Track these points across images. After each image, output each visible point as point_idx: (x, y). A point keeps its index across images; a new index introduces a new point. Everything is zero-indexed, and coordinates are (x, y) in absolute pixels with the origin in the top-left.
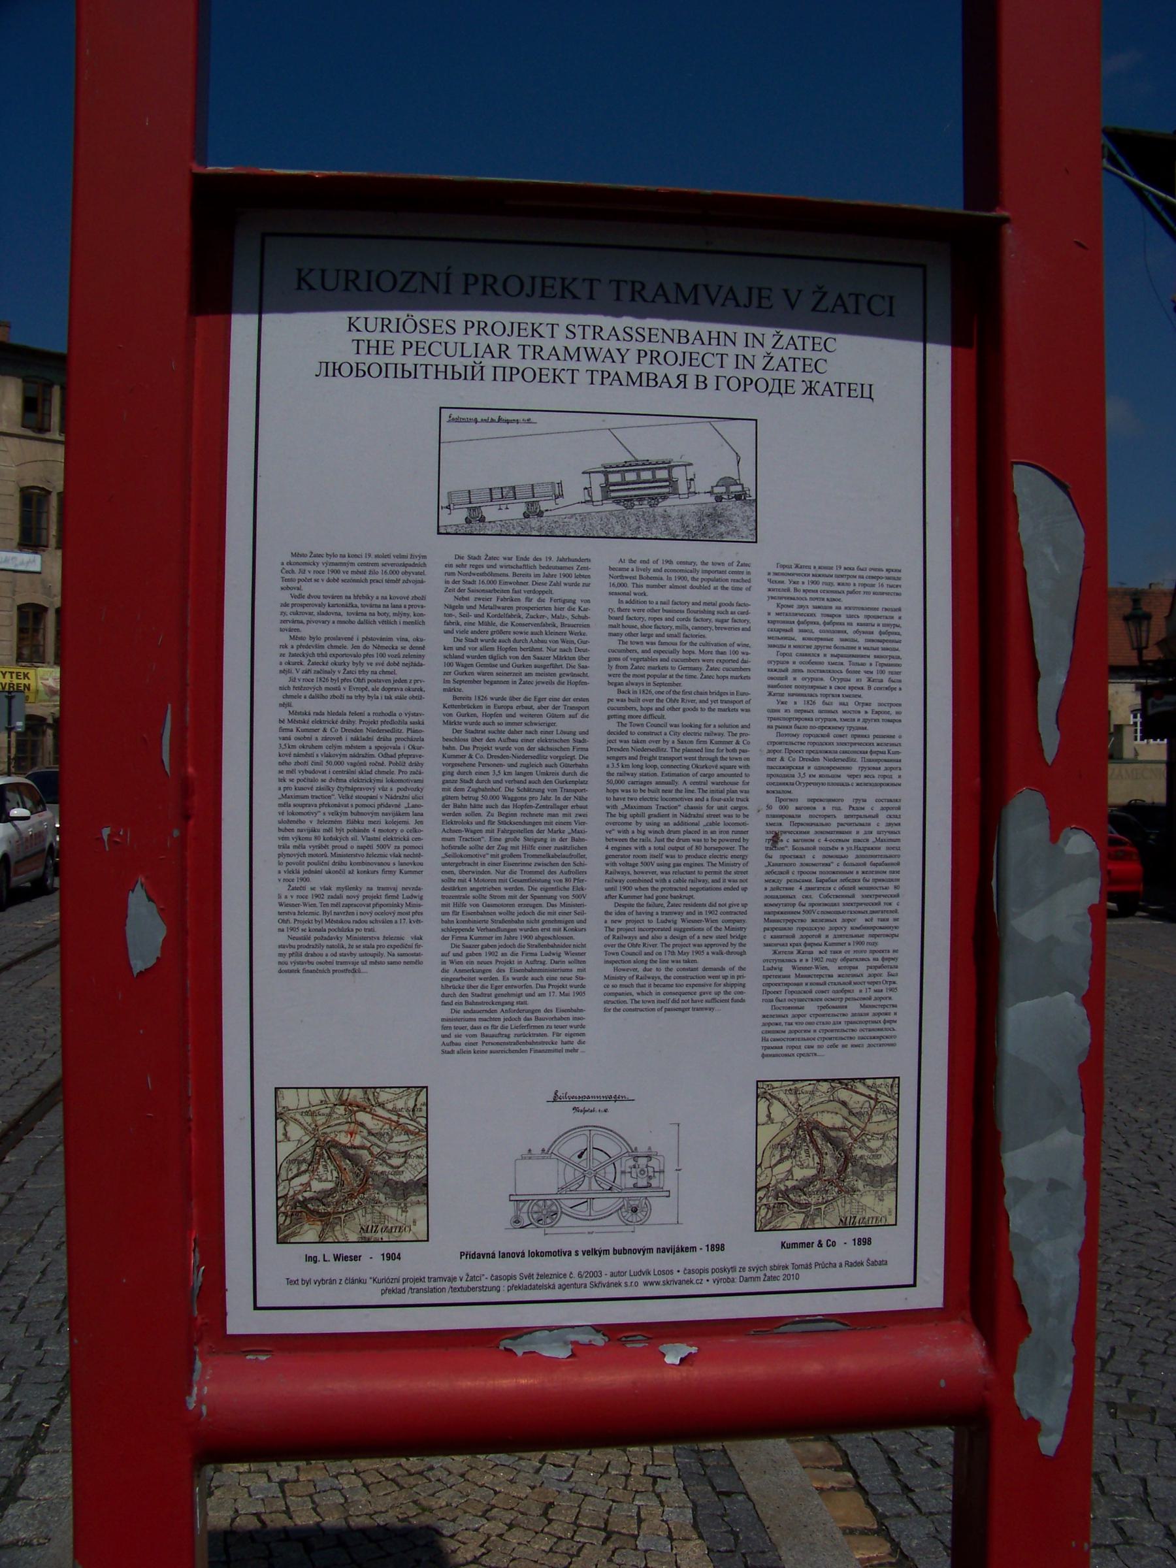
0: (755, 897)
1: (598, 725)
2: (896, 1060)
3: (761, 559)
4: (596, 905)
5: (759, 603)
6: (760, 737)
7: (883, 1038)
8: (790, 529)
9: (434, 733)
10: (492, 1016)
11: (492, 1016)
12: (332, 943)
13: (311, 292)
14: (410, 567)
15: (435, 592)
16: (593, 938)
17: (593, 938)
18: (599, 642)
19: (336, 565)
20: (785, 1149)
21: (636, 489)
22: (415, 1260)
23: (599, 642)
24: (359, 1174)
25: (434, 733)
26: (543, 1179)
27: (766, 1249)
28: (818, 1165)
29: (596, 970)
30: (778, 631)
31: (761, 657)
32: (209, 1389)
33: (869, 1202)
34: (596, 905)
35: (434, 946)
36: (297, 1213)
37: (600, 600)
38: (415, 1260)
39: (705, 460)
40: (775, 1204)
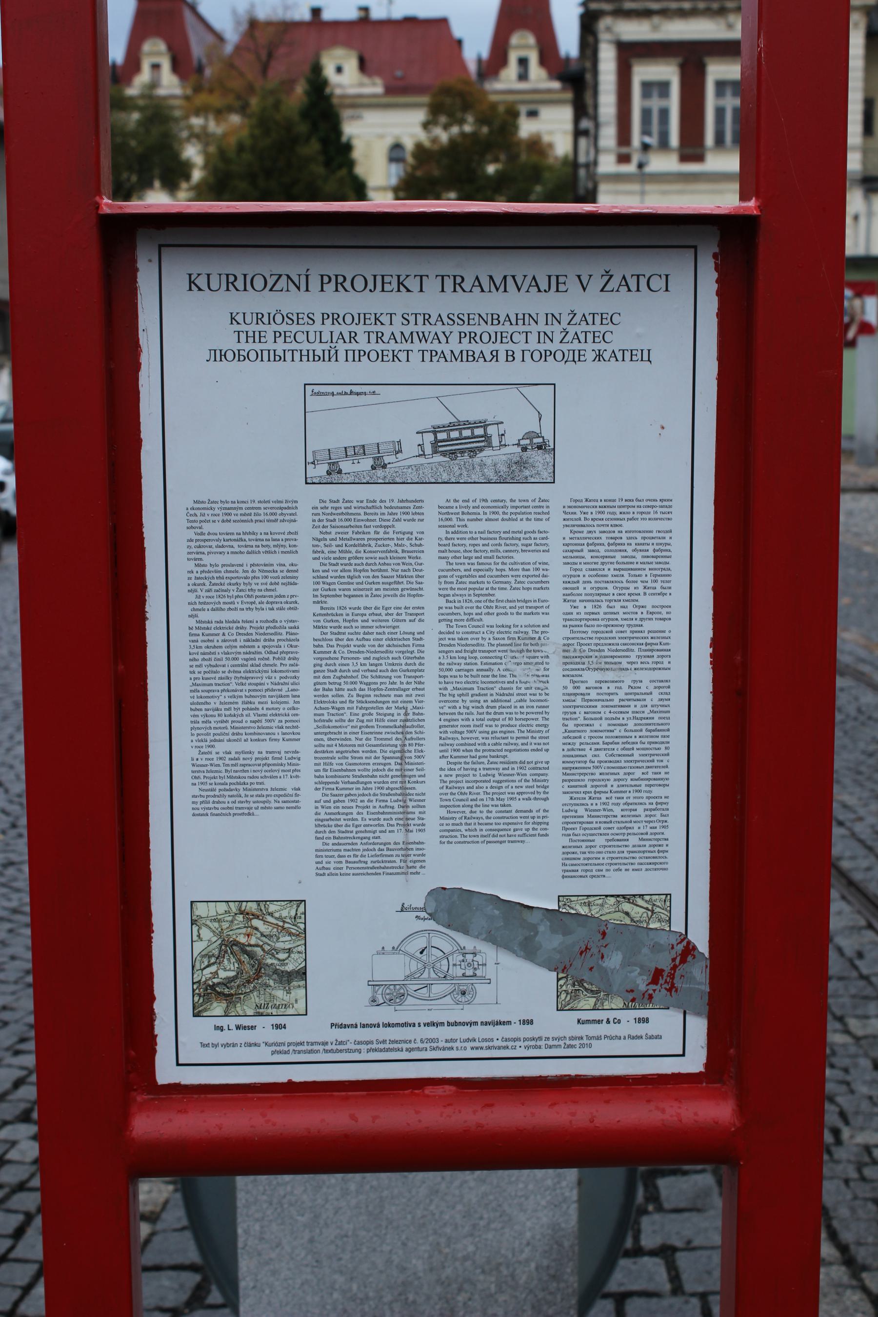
0: (555, 756)
1: (431, 628)
2: (669, 881)
3: (557, 496)
5: (557, 531)
7: (658, 864)
8: (581, 473)
9: (307, 634)
12: (236, 792)
13: (179, 267)
14: (285, 509)
15: (304, 526)
19: (229, 510)
21: (458, 444)
22: (297, 1030)
24: (255, 964)
25: (307, 634)
26: (394, 969)
27: (566, 1024)
30: (571, 552)
31: (557, 571)
35: (309, 795)
37: (431, 529)
38: (297, 1030)
39: (514, 418)
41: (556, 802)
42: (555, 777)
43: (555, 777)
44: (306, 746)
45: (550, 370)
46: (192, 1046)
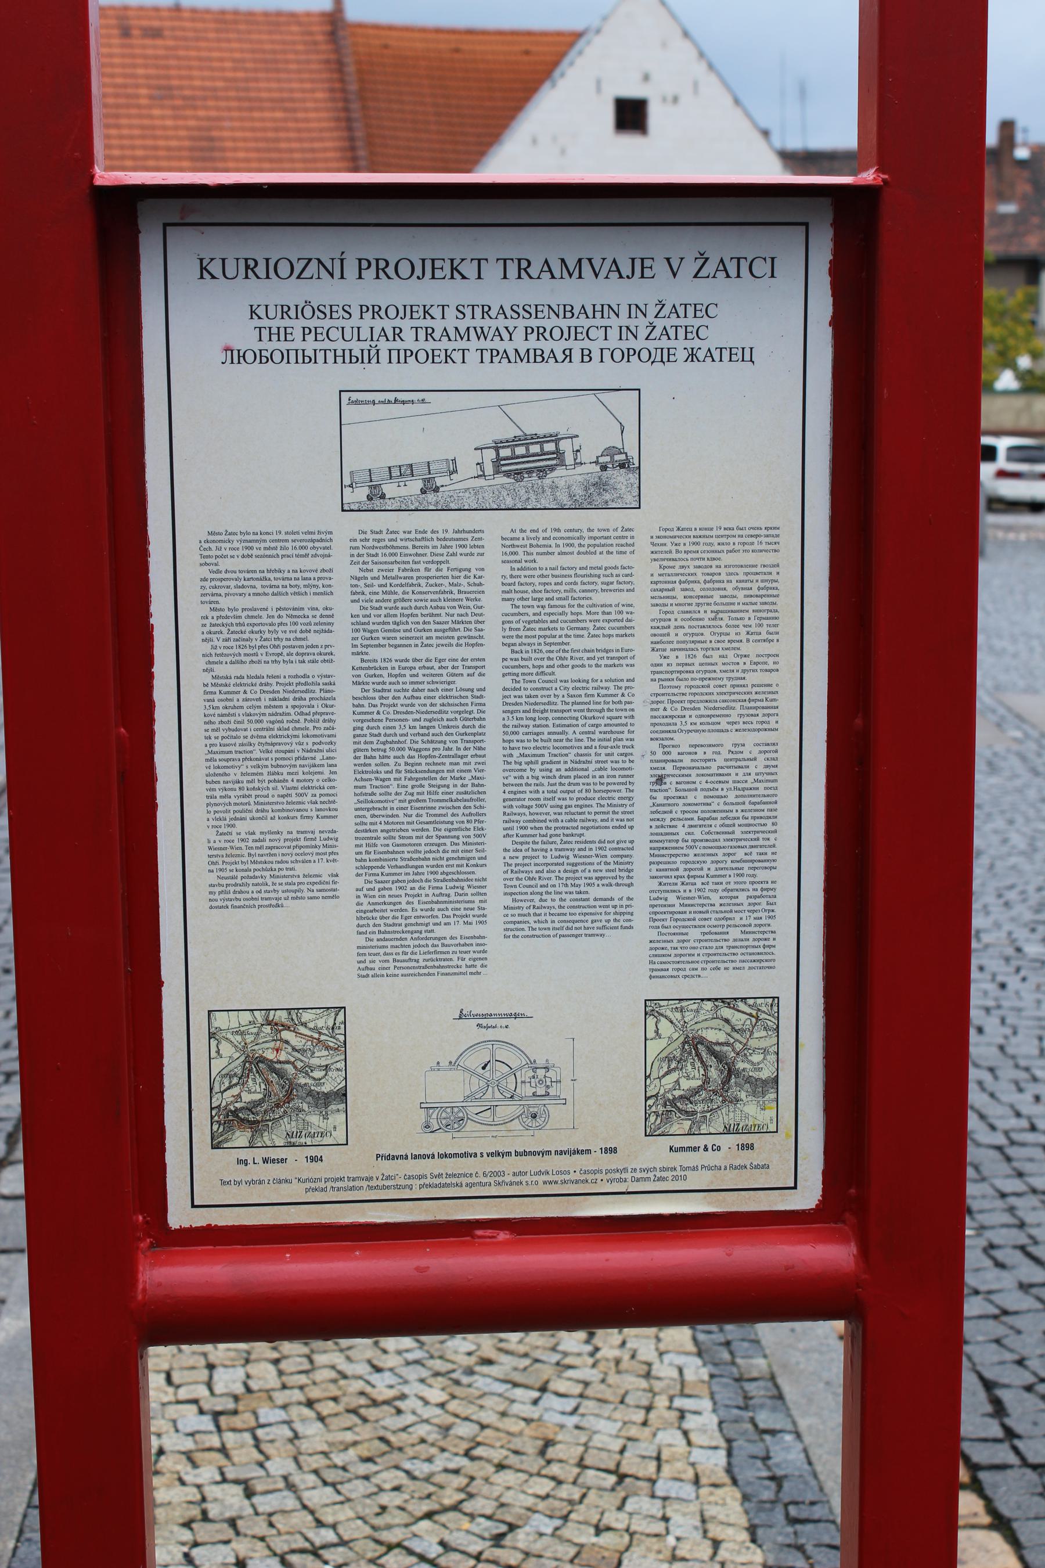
0: (641, 833)
4: (496, 844)
5: (643, 567)
6: (644, 688)
7: (763, 962)
9: (345, 692)
10: (398, 944)
11: (398, 944)
12: (255, 881)
14: (318, 542)
16: (494, 873)
17: (494, 873)
18: (494, 606)
19: (252, 542)
20: (673, 1062)
22: (336, 1162)
23: (494, 606)
24: (284, 1085)
25: (345, 692)
26: (451, 1089)
27: (656, 1153)
28: (705, 1074)
29: (496, 901)
30: (661, 590)
31: (644, 615)
32: (162, 1276)
33: (751, 1110)
34: (496, 844)
35: (349, 883)
36: (230, 1120)
37: (493, 566)
38: (336, 1162)
40: (665, 1111)
41: (641, 891)
42: (641, 856)
43: (641, 856)
44: (345, 824)
45: (635, 372)
46: (206, 1179)
